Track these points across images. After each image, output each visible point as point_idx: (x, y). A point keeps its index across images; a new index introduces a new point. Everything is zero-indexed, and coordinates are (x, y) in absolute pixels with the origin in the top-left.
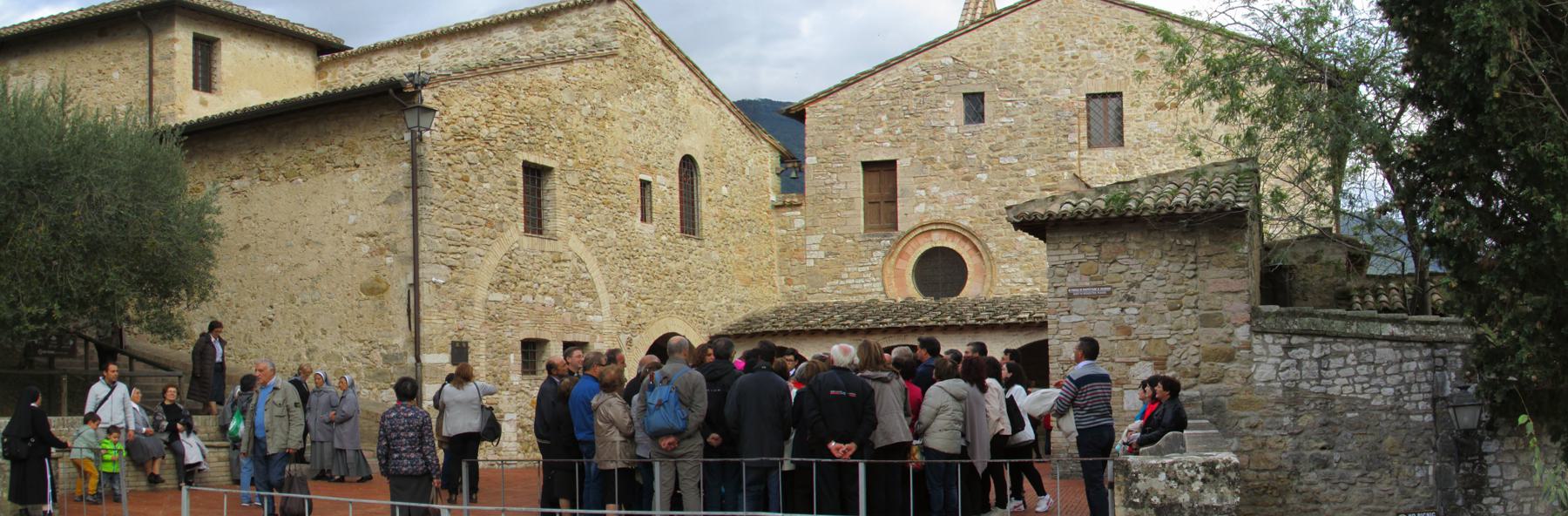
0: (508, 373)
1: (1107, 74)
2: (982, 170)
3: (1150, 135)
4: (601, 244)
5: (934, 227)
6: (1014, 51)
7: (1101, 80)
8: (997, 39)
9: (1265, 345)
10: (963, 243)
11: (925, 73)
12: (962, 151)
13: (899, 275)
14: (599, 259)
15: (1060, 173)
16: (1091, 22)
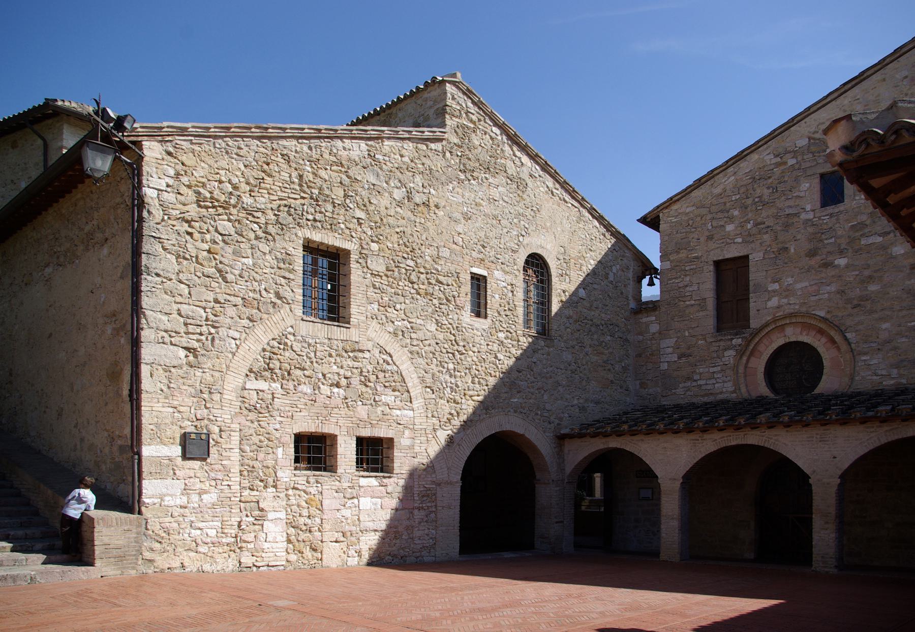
2: (842, 253)
10: (819, 336)
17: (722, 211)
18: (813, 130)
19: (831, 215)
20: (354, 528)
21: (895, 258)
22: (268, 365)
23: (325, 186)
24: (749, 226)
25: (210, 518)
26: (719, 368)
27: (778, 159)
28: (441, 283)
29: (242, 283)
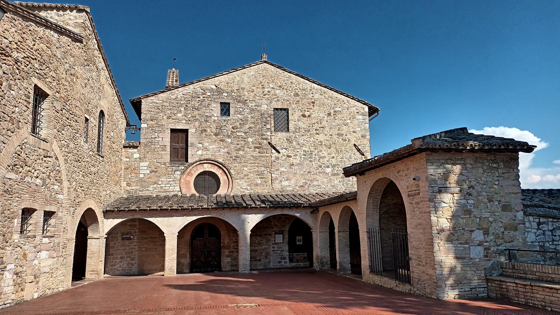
0: (11, 233)
1: (282, 100)
2: (229, 137)
3: (300, 128)
4: (67, 150)
5: (205, 162)
6: (243, 86)
7: (280, 103)
8: (236, 80)
9: (529, 221)
10: (218, 170)
11: (202, 91)
12: (220, 128)
13: (188, 183)
16: (276, 78)
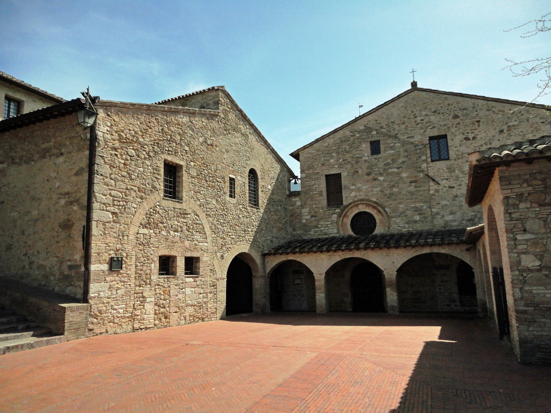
1: (439, 126)
2: (381, 175)
5: (360, 202)
10: (373, 209)
12: (370, 167)
14: (207, 215)
15: (419, 174)
17: (328, 153)
18: (366, 123)
19: (376, 159)
20: (183, 305)
21: (403, 178)
22: (148, 221)
23: (173, 134)
24: (341, 161)
25: (120, 303)
26: (330, 222)
27: (352, 134)
28: (218, 181)
29: (138, 180)
